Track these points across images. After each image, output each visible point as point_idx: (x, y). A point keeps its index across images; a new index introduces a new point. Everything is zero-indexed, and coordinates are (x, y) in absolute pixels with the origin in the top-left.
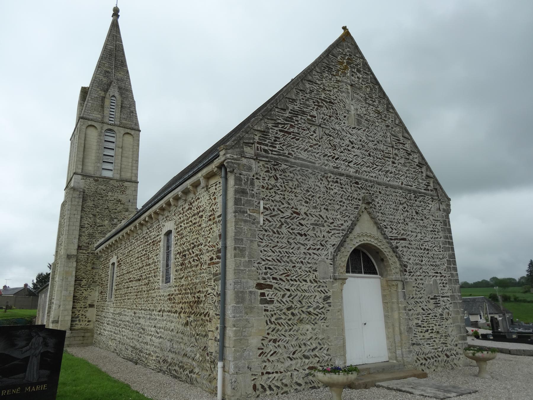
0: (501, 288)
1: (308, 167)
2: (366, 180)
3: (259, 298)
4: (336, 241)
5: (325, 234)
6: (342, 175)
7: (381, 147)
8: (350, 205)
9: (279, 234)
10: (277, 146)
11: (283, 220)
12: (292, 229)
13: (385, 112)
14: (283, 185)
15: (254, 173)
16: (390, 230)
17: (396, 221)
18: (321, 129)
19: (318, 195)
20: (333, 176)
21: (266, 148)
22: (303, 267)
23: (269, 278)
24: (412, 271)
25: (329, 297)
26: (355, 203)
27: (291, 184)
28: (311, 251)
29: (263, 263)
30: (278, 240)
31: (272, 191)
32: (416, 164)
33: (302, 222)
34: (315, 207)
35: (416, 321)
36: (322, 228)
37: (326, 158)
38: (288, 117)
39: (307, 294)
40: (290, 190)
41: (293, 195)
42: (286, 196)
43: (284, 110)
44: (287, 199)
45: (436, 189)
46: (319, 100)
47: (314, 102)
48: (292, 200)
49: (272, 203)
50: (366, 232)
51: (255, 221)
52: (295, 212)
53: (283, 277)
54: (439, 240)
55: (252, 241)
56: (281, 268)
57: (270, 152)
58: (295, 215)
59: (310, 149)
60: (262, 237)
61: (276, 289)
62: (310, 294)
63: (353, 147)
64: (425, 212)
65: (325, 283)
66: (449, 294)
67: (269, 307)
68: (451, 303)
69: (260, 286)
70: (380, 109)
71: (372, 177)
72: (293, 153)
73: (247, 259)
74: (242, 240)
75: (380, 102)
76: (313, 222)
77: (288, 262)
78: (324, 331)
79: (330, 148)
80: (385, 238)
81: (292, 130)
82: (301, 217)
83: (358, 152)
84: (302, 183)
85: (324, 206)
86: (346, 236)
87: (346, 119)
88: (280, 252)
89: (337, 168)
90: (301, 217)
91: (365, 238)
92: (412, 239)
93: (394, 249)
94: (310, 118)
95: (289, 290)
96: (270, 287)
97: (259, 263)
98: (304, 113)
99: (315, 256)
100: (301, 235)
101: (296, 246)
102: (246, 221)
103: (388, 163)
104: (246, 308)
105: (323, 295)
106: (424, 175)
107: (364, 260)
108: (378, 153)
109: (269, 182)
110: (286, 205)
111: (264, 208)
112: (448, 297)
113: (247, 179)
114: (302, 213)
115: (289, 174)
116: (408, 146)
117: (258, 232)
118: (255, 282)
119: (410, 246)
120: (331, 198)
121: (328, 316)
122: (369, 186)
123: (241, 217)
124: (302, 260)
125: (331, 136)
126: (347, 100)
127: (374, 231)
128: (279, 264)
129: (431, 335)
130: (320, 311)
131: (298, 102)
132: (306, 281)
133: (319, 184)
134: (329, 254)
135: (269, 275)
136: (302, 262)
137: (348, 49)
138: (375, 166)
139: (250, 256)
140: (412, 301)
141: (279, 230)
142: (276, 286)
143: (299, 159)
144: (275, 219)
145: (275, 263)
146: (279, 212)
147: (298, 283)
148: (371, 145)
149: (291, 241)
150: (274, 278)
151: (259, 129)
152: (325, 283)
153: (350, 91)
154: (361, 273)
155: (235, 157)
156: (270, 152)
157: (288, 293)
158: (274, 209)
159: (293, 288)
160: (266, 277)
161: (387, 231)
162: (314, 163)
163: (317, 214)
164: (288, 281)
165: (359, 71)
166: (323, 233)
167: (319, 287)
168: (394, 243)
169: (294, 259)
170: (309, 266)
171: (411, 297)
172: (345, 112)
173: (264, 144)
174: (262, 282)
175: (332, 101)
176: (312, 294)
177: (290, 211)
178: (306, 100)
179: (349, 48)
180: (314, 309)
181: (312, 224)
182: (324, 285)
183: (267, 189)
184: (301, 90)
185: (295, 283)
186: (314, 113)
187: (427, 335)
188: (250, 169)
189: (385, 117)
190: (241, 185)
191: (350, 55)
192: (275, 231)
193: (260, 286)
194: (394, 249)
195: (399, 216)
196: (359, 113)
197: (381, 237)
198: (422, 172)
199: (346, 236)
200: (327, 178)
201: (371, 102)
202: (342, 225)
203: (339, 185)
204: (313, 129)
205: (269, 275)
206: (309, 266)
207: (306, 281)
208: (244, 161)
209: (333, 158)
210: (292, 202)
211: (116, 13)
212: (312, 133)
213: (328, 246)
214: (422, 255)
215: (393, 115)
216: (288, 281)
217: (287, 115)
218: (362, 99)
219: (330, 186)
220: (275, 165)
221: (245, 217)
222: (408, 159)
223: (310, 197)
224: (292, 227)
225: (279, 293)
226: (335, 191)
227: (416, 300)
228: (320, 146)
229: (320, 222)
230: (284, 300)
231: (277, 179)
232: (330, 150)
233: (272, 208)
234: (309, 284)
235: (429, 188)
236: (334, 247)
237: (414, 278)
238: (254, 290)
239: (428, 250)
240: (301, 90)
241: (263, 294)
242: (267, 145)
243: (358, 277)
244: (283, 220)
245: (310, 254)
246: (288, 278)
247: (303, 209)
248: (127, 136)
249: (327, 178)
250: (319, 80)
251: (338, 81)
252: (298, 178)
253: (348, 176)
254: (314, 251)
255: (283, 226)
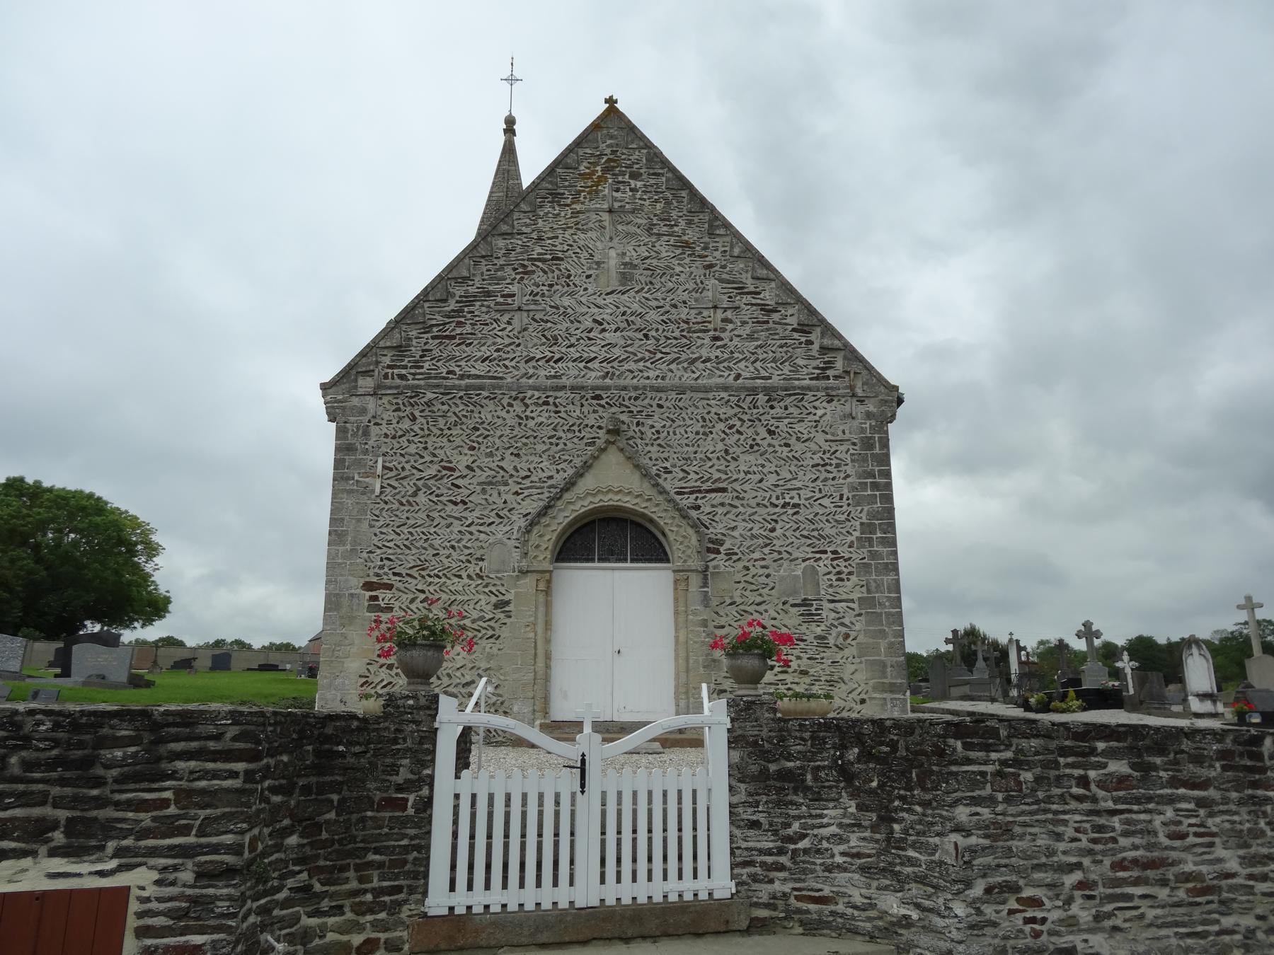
1: (482, 388)
2: (625, 388)
3: (366, 604)
4: (532, 506)
5: (510, 497)
8: (575, 440)
9: (410, 504)
10: (426, 365)
11: (420, 483)
12: (437, 496)
13: (706, 239)
14: (425, 426)
15: (369, 416)
16: (682, 475)
17: (702, 456)
18: (525, 314)
19: (499, 433)
20: (537, 394)
21: (404, 372)
22: (454, 554)
23: (386, 574)
24: (736, 550)
25: (508, 603)
26: (588, 436)
27: (441, 422)
28: (472, 529)
29: (379, 551)
30: (408, 515)
31: (404, 439)
32: (790, 328)
33: (460, 482)
34: (491, 455)
36: (502, 488)
37: (533, 363)
38: (453, 311)
39: (459, 598)
40: (439, 432)
41: (445, 440)
42: (429, 445)
43: (445, 301)
44: (431, 449)
46: (526, 263)
47: (515, 269)
48: (441, 448)
49: (402, 459)
50: (613, 484)
51: (366, 490)
52: (445, 468)
53: (412, 572)
54: (841, 481)
55: (359, 521)
56: (410, 558)
57: (410, 377)
58: (444, 472)
59: (495, 355)
60: (377, 513)
61: (398, 590)
62: (466, 598)
63: (604, 330)
65: (499, 578)
66: (855, 596)
68: (860, 615)
69: (368, 586)
70: (691, 236)
71: (648, 378)
72: (457, 369)
73: (349, 547)
74: (343, 520)
75: (690, 223)
76: (483, 479)
77: (425, 549)
78: (490, 657)
79: (544, 344)
80: (661, 493)
81: (458, 331)
82: (457, 474)
83: (610, 337)
84: (465, 416)
85: (512, 450)
87: (591, 280)
88: (410, 533)
89: (555, 377)
90: (457, 474)
94: (502, 300)
95: (423, 592)
96: (389, 587)
97: (370, 552)
98: (488, 294)
99: (482, 536)
100: (455, 504)
101: (444, 522)
102: (350, 492)
103: (700, 342)
104: (342, 617)
105: (494, 599)
107: (611, 536)
108: (673, 326)
109: (400, 425)
110: (428, 458)
111: (384, 467)
112: (852, 601)
113: (358, 428)
114: (461, 466)
115: (440, 407)
116: (769, 295)
117: (371, 506)
118: (362, 581)
119: (736, 502)
120: (531, 433)
121: (504, 633)
122: (630, 399)
123: (343, 486)
124: (453, 543)
125: (547, 321)
126: (598, 244)
127: (634, 481)
128: (407, 551)
129: (781, 677)
130: (485, 625)
131: (477, 279)
132: (469, 577)
133: (503, 414)
134: (515, 531)
135: (386, 570)
136: (453, 547)
137: (609, 142)
138: (659, 355)
139: (354, 543)
141: (411, 499)
142: (400, 585)
143: (469, 377)
144: (405, 483)
145: (399, 551)
146: (414, 471)
147: (444, 579)
149: (435, 514)
150: (395, 574)
151: (388, 344)
152: (499, 578)
153: (606, 224)
154: (625, 560)
155: (340, 397)
156: (410, 377)
157: (422, 596)
158: (403, 468)
159: (431, 589)
160: (381, 572)
162: (501, 378)
163: (493, 465)
164: (423, 577)
166: (504, 497)
167: (486, 586)
169: (436, 543)
170: (468, 552)
171: (728, 601)
172: (590, 268)
173: (399, 367)
174: (375, 579)
175: (560, 255)
176: (472, 597)
177: (436, 467)
178: (497, 270)
179: (611, 137)
180: (474, 621)
181: (479, 484)
182: (498, 583)
183: (394, 437)
184: (483, 257)
185: (437, 580)
186: (514, 289)
188: (363, 411)
189: (705, 248)
190: (346, 438)
191: (613, 152)
192: (404, 501)
193: (368, 586)
196: (627, 260)
197: (649, 491)
198: (810, 343)
200: (522, 400)
201: (665, 229)
202: (551, 477)
203: (552, 408)
204: (506, 318)
205: (386, 570)
206: (468, 552)
207: (460, 577)
208: (355, 401)
209: (547, 361)
210: (442, 452)
211: (510, 127)
212: (503, 326)
213: (514, 518)
214: (774, 517)
215: (728, 239)
216: (423, 577)
218: (639, 231)
219: (528, 413)
220: (411, 397)
221: (351, 485)
222: (767, 322)
223: (480, 439)
224: (438, 492)
225: (404, 596)
226: (540, 420)
227: (742, 607)
228: (519, 345)
229: (499, 478)
230: (413, 607)
231: (414, 419)
232: (541, 348)
233: (399, 467)
234: (466, 581)
236: (529, 517)
237: (740, 565)
238: (359, 591)
239: (795, 506)
240: (483, 257)
242: (405, 367)
243: (613, 569)
244: (420, 483)
245: (471, 533)
246: (423, 573)
247: (462, 462)
249: (522, 400)
250: (527, 225)
251: (576, 213)
252: (457, 410)
254: (481, 528)
255: (420, 493)
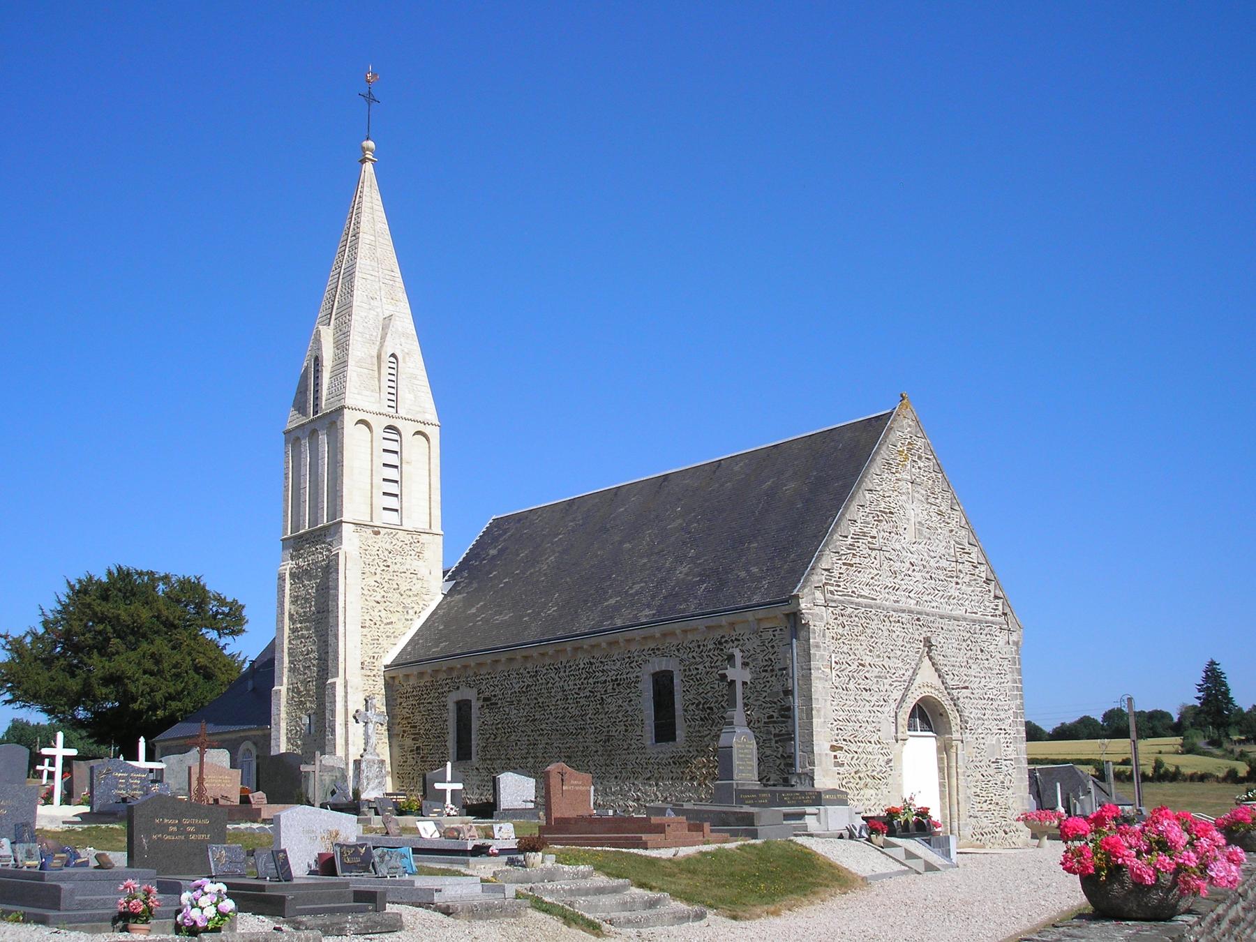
0: (236, 675)
4: (897, 695)
6: (903, 611)
7: (944, 563)
34: (879, 656)
35: (974, 790)
45: (1005, 614)
50: (926, 683)
64: (992, 648)
66: (1012, 757)
67: (841, 770)
69: (833, 748)
86: (907, 689)
91: (926, 689)
92: (976, 686)
93: (955, 701)
96: (841, 749)
106: (992, 594)
107: (927, 716)
127: (937, 682)
140: (972, 765)
148: (932, 562)
161: (948, 678)
165: (920, 458)
168: (955, 692)
187: (985, 806)
194: (955, 701)
195: (961, 658)
199: (907, 689)
217: (850, 541)
235: (997, 612)
241: (835, 757)
248: (361, 426)
253: (910, 612)
